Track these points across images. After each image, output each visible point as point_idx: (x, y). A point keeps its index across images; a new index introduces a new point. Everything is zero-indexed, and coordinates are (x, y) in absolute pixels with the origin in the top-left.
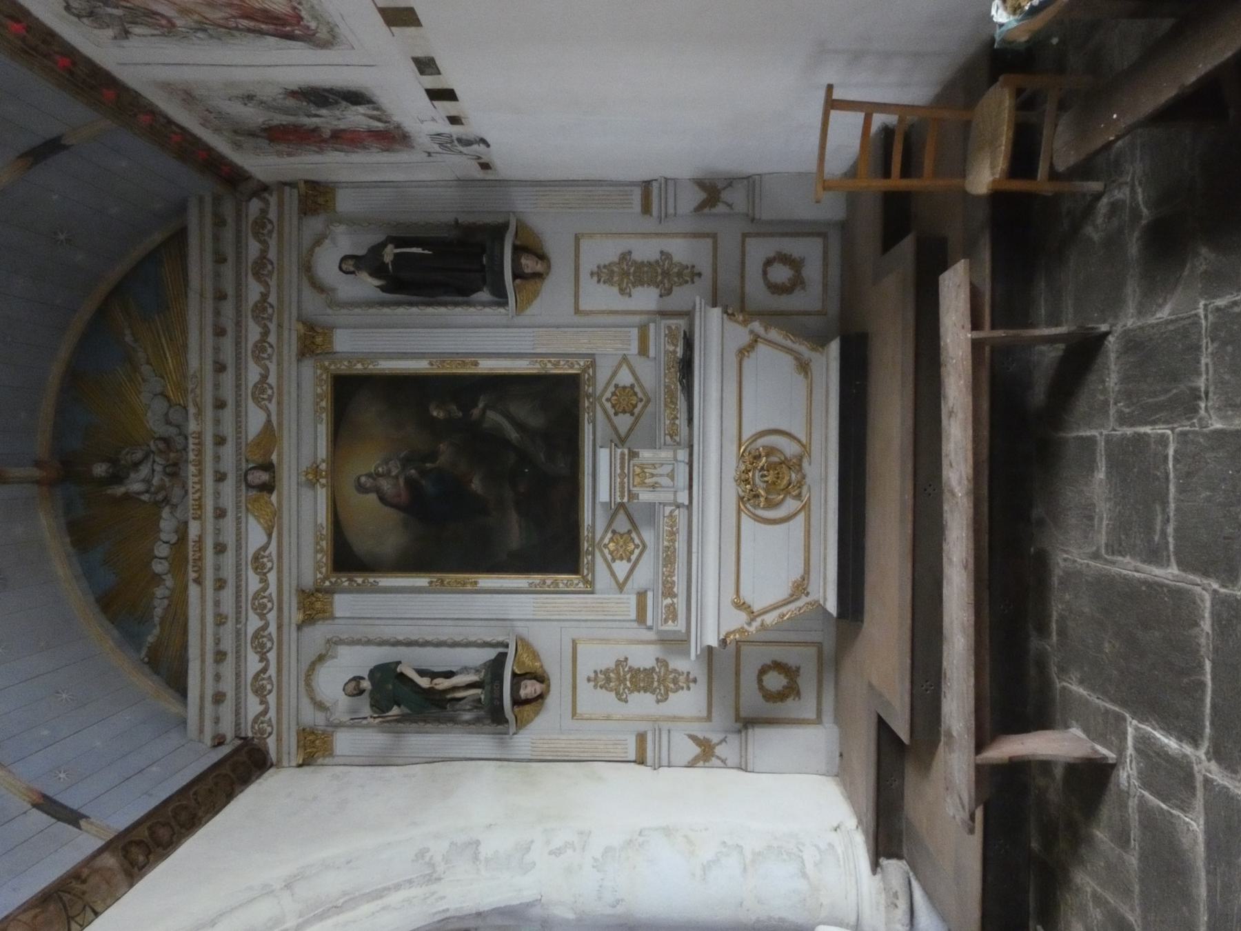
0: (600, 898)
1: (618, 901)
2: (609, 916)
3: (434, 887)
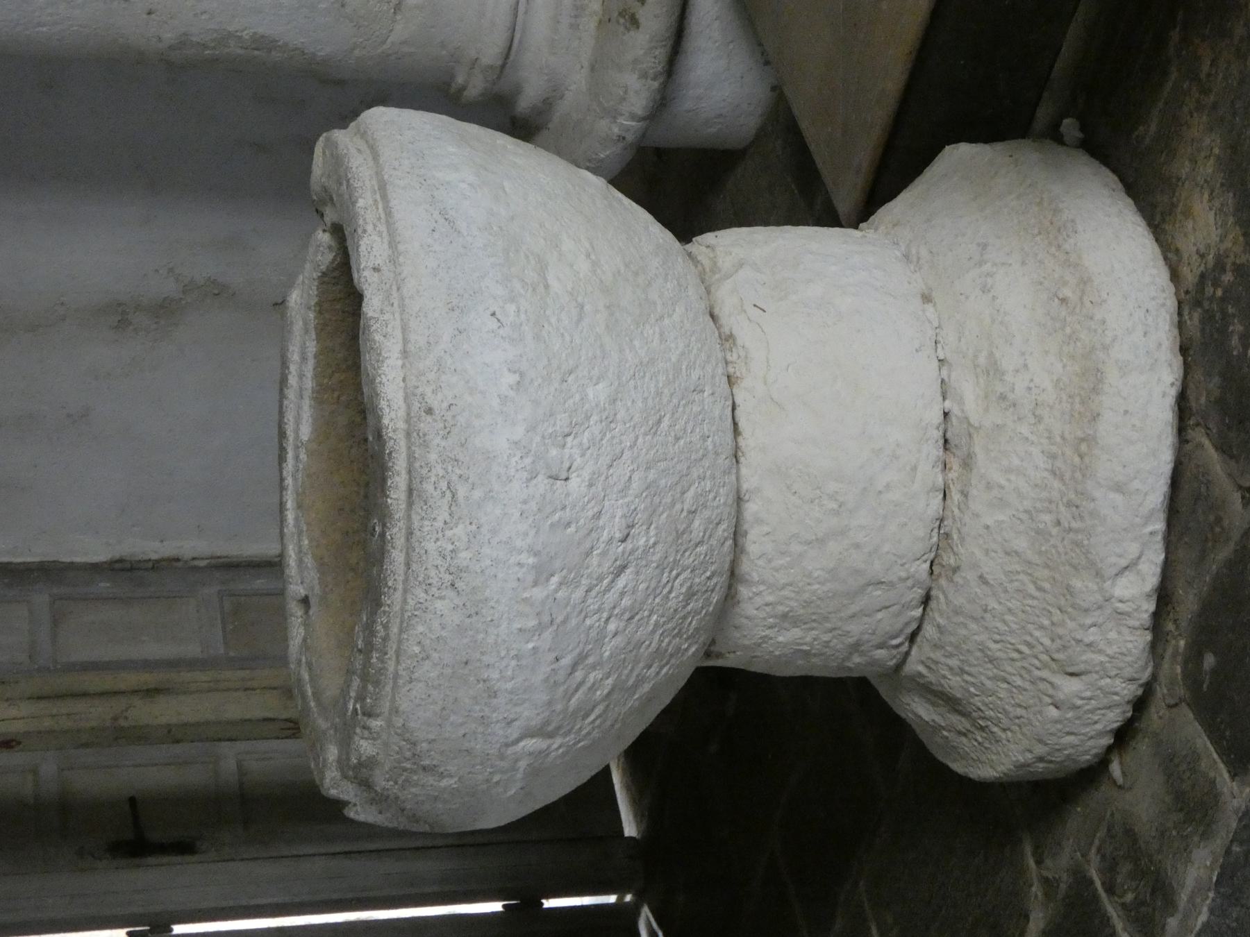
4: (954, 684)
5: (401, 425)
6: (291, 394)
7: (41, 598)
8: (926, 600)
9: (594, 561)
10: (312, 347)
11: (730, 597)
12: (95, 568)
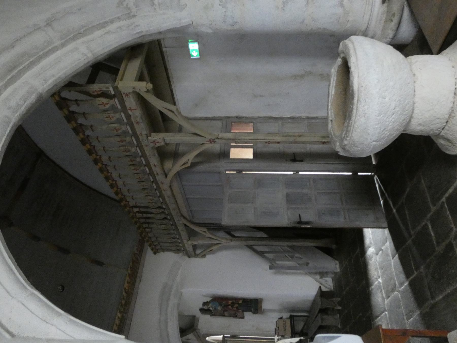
0: (225, 22)
1: (235, 23)
2: (231, 30)
3: (132, 20)
4: (450, 137)
5: (357, 89)
6: (331, 86)
7: (280, 122)
8: (447, 122)
9: (389, 112)
10: (335, 78)
11: (410, 121)
12: (288, 118)
